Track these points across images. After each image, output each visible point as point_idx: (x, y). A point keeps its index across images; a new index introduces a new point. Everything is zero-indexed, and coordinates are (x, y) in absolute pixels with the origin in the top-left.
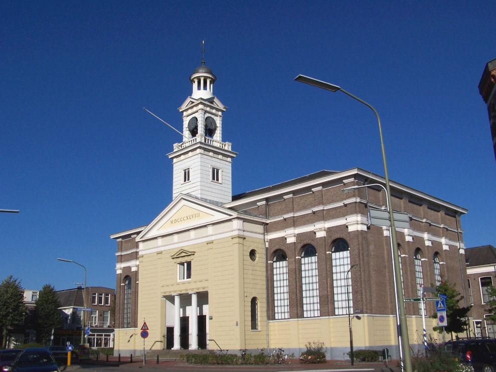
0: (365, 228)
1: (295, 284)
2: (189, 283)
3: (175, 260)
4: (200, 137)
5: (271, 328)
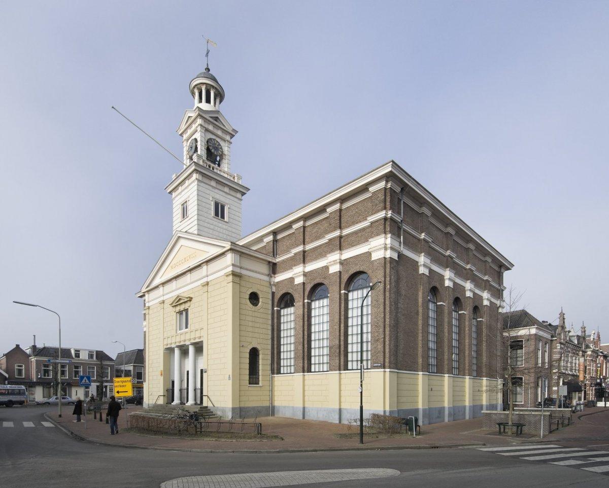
0: (395, 256)
1: (302, 333)
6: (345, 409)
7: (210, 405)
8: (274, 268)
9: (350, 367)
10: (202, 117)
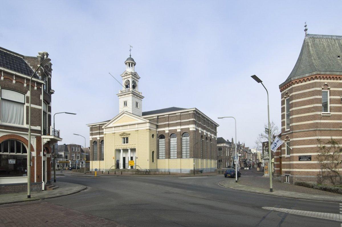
2: (127, 145)
3: (121, 136)
4: (131, 89)
5: (158, 162)
6: (183, 169)
7: (139, 168)
8: (158, 127)
9: (171, 158)
10: (131, 74)
